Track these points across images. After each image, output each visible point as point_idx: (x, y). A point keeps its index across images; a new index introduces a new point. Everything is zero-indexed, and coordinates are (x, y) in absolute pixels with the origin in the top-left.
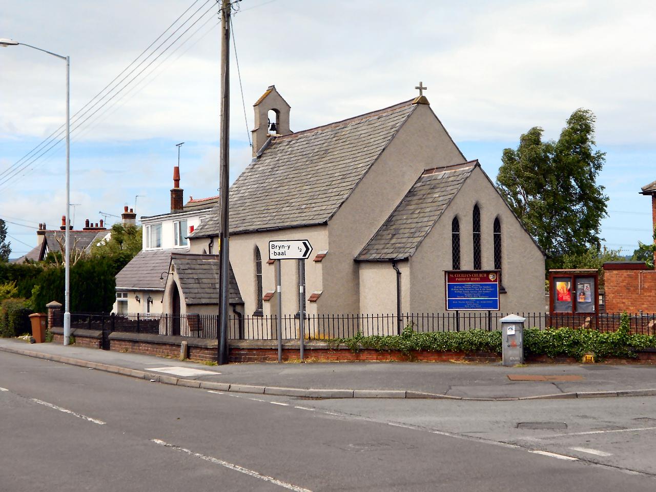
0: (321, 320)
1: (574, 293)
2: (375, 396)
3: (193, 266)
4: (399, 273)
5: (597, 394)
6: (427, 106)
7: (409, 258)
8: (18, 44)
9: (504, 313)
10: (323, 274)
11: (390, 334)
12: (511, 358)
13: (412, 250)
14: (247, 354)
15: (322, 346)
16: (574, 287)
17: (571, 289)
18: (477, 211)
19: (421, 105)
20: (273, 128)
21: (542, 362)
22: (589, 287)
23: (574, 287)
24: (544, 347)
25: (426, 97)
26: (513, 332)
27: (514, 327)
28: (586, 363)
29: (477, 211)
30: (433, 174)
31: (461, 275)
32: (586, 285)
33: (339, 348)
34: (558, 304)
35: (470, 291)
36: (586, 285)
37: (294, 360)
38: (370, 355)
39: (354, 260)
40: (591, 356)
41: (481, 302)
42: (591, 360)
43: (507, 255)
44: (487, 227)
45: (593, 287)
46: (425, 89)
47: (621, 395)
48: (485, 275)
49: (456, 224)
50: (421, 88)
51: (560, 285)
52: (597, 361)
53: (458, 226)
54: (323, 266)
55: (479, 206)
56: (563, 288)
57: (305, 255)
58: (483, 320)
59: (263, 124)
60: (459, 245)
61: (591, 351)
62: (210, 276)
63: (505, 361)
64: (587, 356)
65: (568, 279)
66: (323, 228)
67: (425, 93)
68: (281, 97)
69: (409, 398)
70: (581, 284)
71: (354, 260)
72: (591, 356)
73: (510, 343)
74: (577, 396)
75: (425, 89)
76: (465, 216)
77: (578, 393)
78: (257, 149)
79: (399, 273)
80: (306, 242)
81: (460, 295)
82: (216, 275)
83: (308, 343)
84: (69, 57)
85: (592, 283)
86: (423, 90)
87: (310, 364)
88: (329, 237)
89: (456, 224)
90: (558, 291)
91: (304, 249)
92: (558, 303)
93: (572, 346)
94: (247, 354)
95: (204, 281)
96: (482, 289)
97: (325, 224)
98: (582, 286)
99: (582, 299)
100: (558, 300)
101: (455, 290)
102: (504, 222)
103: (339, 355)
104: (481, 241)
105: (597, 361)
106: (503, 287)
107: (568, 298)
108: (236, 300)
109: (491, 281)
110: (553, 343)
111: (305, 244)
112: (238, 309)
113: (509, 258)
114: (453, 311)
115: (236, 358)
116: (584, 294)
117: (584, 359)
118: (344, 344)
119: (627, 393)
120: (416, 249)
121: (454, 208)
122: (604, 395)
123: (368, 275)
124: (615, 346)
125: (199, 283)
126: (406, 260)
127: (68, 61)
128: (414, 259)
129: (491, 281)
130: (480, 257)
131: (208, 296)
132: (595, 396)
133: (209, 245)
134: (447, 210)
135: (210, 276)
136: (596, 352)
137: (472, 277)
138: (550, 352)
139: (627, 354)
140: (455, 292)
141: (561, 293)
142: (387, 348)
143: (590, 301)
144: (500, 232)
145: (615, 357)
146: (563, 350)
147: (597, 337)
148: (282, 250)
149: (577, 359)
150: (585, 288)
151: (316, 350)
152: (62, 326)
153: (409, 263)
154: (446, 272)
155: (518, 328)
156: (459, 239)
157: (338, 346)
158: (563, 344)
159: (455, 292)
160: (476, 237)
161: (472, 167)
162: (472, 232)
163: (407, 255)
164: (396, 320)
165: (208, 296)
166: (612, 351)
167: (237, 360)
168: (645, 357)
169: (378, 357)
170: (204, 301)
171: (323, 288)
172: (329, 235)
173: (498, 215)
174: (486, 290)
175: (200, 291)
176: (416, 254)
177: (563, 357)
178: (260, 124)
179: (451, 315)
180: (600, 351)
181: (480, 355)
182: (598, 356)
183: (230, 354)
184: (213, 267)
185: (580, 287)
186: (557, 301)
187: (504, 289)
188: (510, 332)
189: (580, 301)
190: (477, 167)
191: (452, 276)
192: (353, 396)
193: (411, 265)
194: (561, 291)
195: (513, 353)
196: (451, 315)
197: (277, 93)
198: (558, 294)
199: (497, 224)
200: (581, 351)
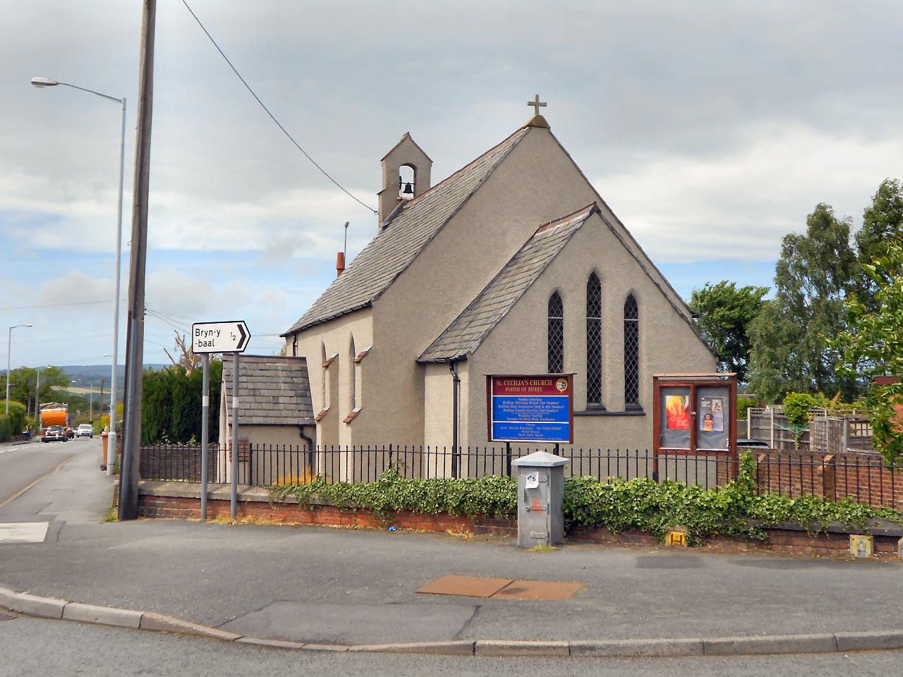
0: (357, 454)
1: (694, 415)
2: (93, 621)
3: (250, 372)
4: (457, 381)
5: (521, 648)
6: (546, 130)
7: (468, 356)
8: (58, 84)
9: (524, 451)
10: (362, 381)
11: (440, 476)
12: (532, 533)
13: (475, 345)
14: (163, 505)
15: (262, 497)
16: (695, 405)
17: (690, 408)
18: (594, 285)
19: (537, 129)
20: (408, 190)
21: (598, 542)
22: (720, 404)
23: (695, 405)
24: (599, 514)
25: (545, 117)
26: (535, 485)
27: (537, 475)
28: (672, 547)
29: (594, 285)
30: (547, 231)
31: (513, 383)
32: (715, 402)
33: (287, 501)
34: (667, 434)
35: (526, 409)
36: (715, 402)
37: (225, 517)
38: (330, 516)
39: (416, 361)
40: (682, 534)
41: (544, 428)
42: (681, 542)
43: (648, 354)
44: (612, 310)
45: (727, 405)
46: (544, 105)
47: (577, 653)
48: (550, 383)
49: (556, 303)
50: (536, 104)
51: (671, 401)
52: (691, 544)
53: (561, 307)
54: (362, 369)
55: (599, 276)
56: (676, 406)
57: (239, 346)
58: (498, 459)
59: (392, 183)
60: (561, 338)
61: (681, 523)
62: (274, 386)
63: (522, 539)
64: (674, 533)
65: (686, 391)
66: (366, 312)
67: (542, 111)
68: (419, 148)
69: (144, 629)
70: (707, 399)
71: (416, 361)
72: (682, 534)
73: (530, 505)
74: (474, 651)
75: (544, 105)
76: (571, 291)
77: (479, 643)
78: (383, 216)
79: (457, 381)
80: (242, 324)
81: (516, 416)
82: (282, 385)
83: (245, 490)
84: (125, 99)
85: (726, 399)
86: (534, 101)
87: (222, 527)
88: (374, 326)
89: (556, 303)
90: (668, 411)
91: (239, 336)
92: (667, 431)
93: (649, 515)
94: (163, 505)
95: (263, 392)
96: (545, 405)
97: (368, 306)
98: (708, 403)
99: (708, 426)
100: (668, 428)
101: (504, 407)
102: (642, 302)
103: (287, 513)
104: (602, 331)
105: (691, 544)
106: (640, 406)
107: (684, 423)
108: (306, 421)
109: (559, 393)
110: (615, 507)
111: (240, 327)
112: (308, 432)
113: (649, 360)
114: (499, 445)
115: (150, 511)
116: (712, 417)
117: (668, 539)
118: (293, 496)
119: (592, 648)
120: (481, 343)
121: (552, 278)
122: (537, 652)
123: (438, 384)
124: (725, 516)
125: (254, 396)
126: (463, 359)
127: (125, 104)
128: (477, 357)
129: (559, 393)
130: (600, 357)
131: (264, 413)
132: (517, 652)
133: (294, 344)
134: (539, 280)
135: (274, 386)
136: (690, 527)
137: (531, 386)
138: (611, 523)
139: (746, 533)
140: (505, 410)
141: (673, 415)
142: (352, 505)
143: (721, 429)
144: (637, 318)
145: (726, 537)
146: (633, 520)
147: (695, 497)
148: (209, 338)
149: (657, 536)
150: (714, 406)
151: (255, 503)
152: (770, 436)
153: (468, 364)
154: (489, 377)
155: (545, 477)
156: (562, 328)
157: (284, 497)
158: (632, 508)
159: (505, 410)
160: (593, 325)
161: (587, 214)
162: (584, 317)
163: (461, 353)
164: (449, 458)
165: (264, 413)
166: (720, 525)
167: (151, 514)
168: (782, 540)
169: (343, 519)
170: (255, 421)
171: (362, 404)
172: (374, 322)
173: (633, 290)
174: (551, 409)
175: (253, 406)
176: (480, 350)
177: (634, 533)
178: (387, 184)
179: (498, 451)
180: (697, 524)
181: (497, 523)
182: (694, 535)
183: (139, 504)
184: (280, 373)
185: (704, 404)
186: (666, 429)
187: (642, 409)
188: (531, 484)
189: (706, 429)
190: (595, 215)
191: (499, 383)
192: (60, 616)
193: (471, 366)
194: (675, 413)
195: (536, 523)
196: (498, 451)
197: (413, 142)
198: (668, 417)
199: (631, 306)
200: (664, 523)
